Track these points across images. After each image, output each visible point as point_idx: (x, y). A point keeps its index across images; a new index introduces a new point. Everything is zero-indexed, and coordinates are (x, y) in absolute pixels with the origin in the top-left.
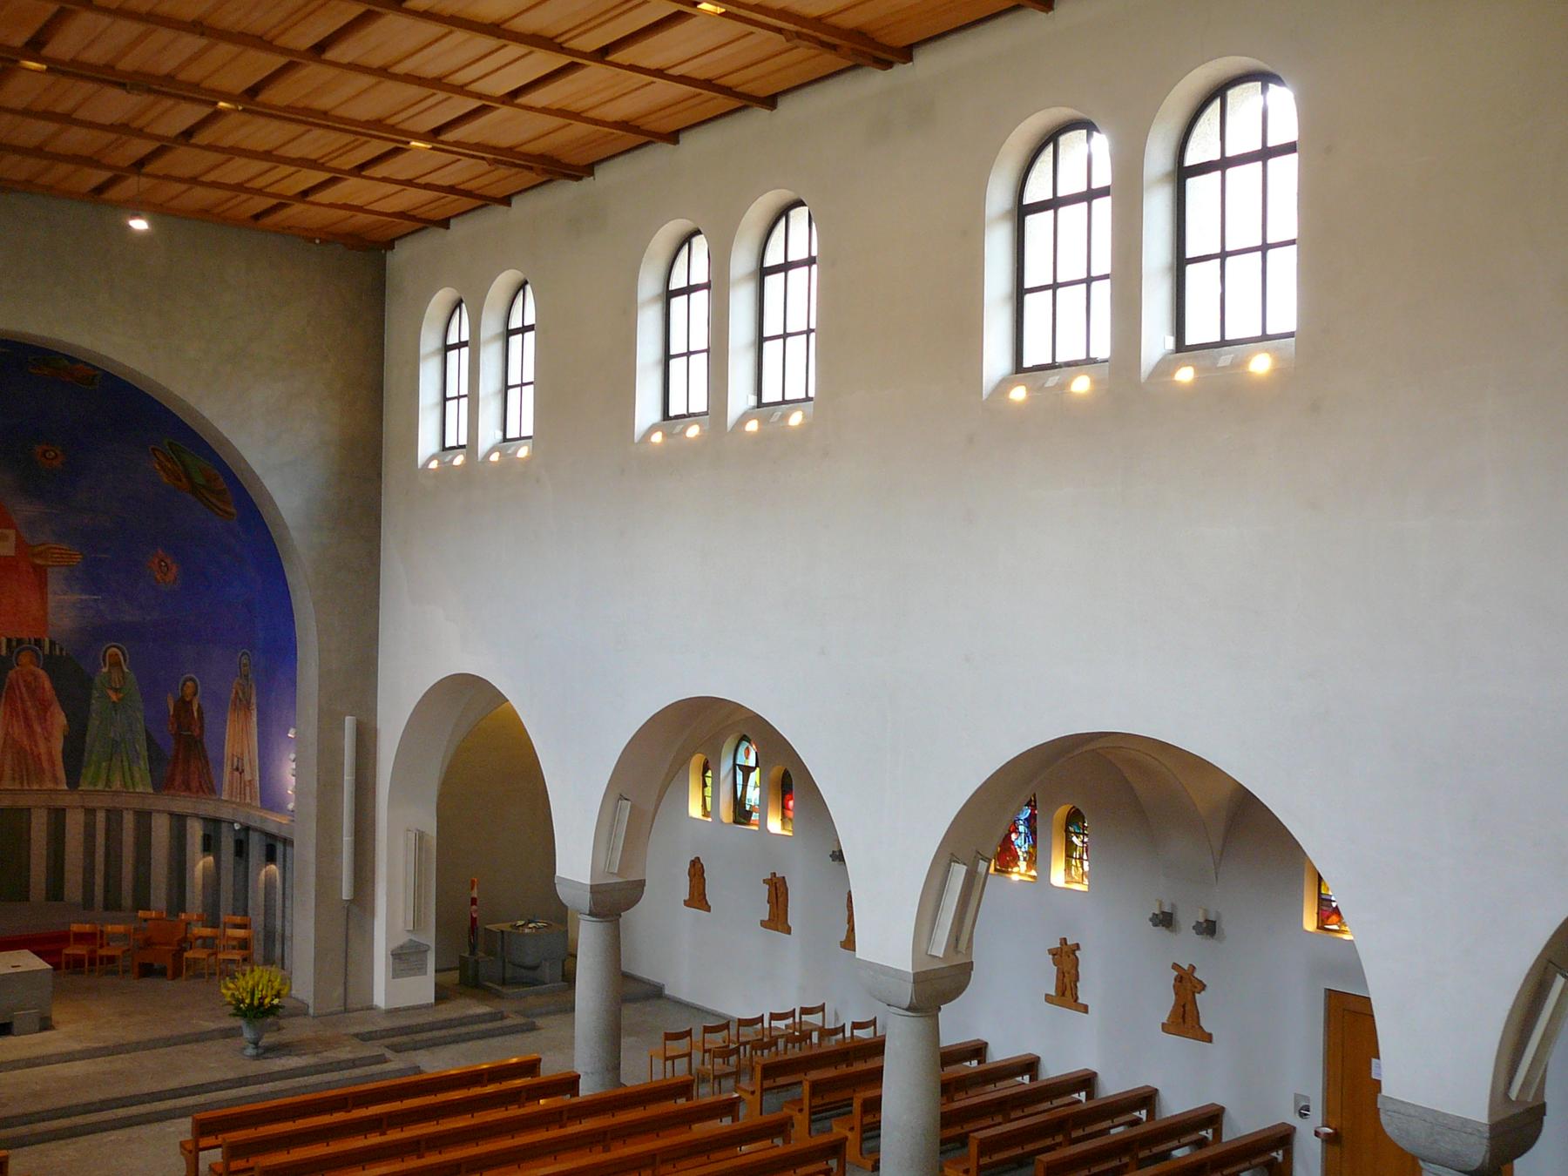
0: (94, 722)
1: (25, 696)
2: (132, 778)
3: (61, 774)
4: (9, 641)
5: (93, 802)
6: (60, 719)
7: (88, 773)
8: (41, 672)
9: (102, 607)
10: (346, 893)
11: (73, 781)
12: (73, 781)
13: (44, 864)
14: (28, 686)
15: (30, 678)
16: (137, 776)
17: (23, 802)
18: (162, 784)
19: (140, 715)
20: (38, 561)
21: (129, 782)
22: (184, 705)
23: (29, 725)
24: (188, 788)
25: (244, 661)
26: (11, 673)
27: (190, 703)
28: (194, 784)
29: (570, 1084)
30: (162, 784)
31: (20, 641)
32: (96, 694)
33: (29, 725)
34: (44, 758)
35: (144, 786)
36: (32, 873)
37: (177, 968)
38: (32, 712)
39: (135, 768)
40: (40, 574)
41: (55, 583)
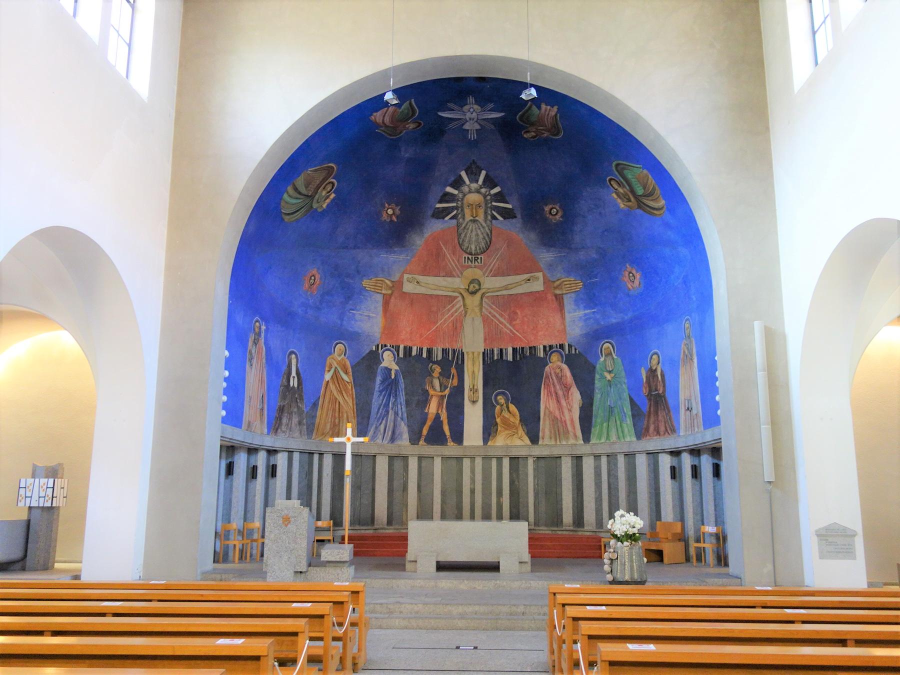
0: (597, 396)
1: (555, 381)
2: (623, 432)
3: (579, 433)
4: (545, 347)
5: (598, 451)
6: (576, 396)
7: (595, 431)
8: (565, 367)
9: (598, 316)
10: (769, 476)
11: (587, 438)
12: (587, 438)
13: (571, 496)
14: (557, 376)
15: (558, 371)
16: (626, 430)
17: (556, 452)
18: (641, 433)
19: (625, 387)
20: (558, 292)
21: (621, 435)
22: (652, 372)
23: (558, 401)
24: (658, 433)
25: (687, 325)
26: (547, 368)
27: (656, 370)
28: (662, 429)
29: (611, 516)
30: (641, 433)
31: (551, 347)
32: (597, 376)
33: (558, 401)
34: (568, 423)
35: (630, 437)
36: (564, 502)
37: (228, 447)
38: (560, 393)
39: (624, 425)
40: (559, 299)
41: (568, 302)
